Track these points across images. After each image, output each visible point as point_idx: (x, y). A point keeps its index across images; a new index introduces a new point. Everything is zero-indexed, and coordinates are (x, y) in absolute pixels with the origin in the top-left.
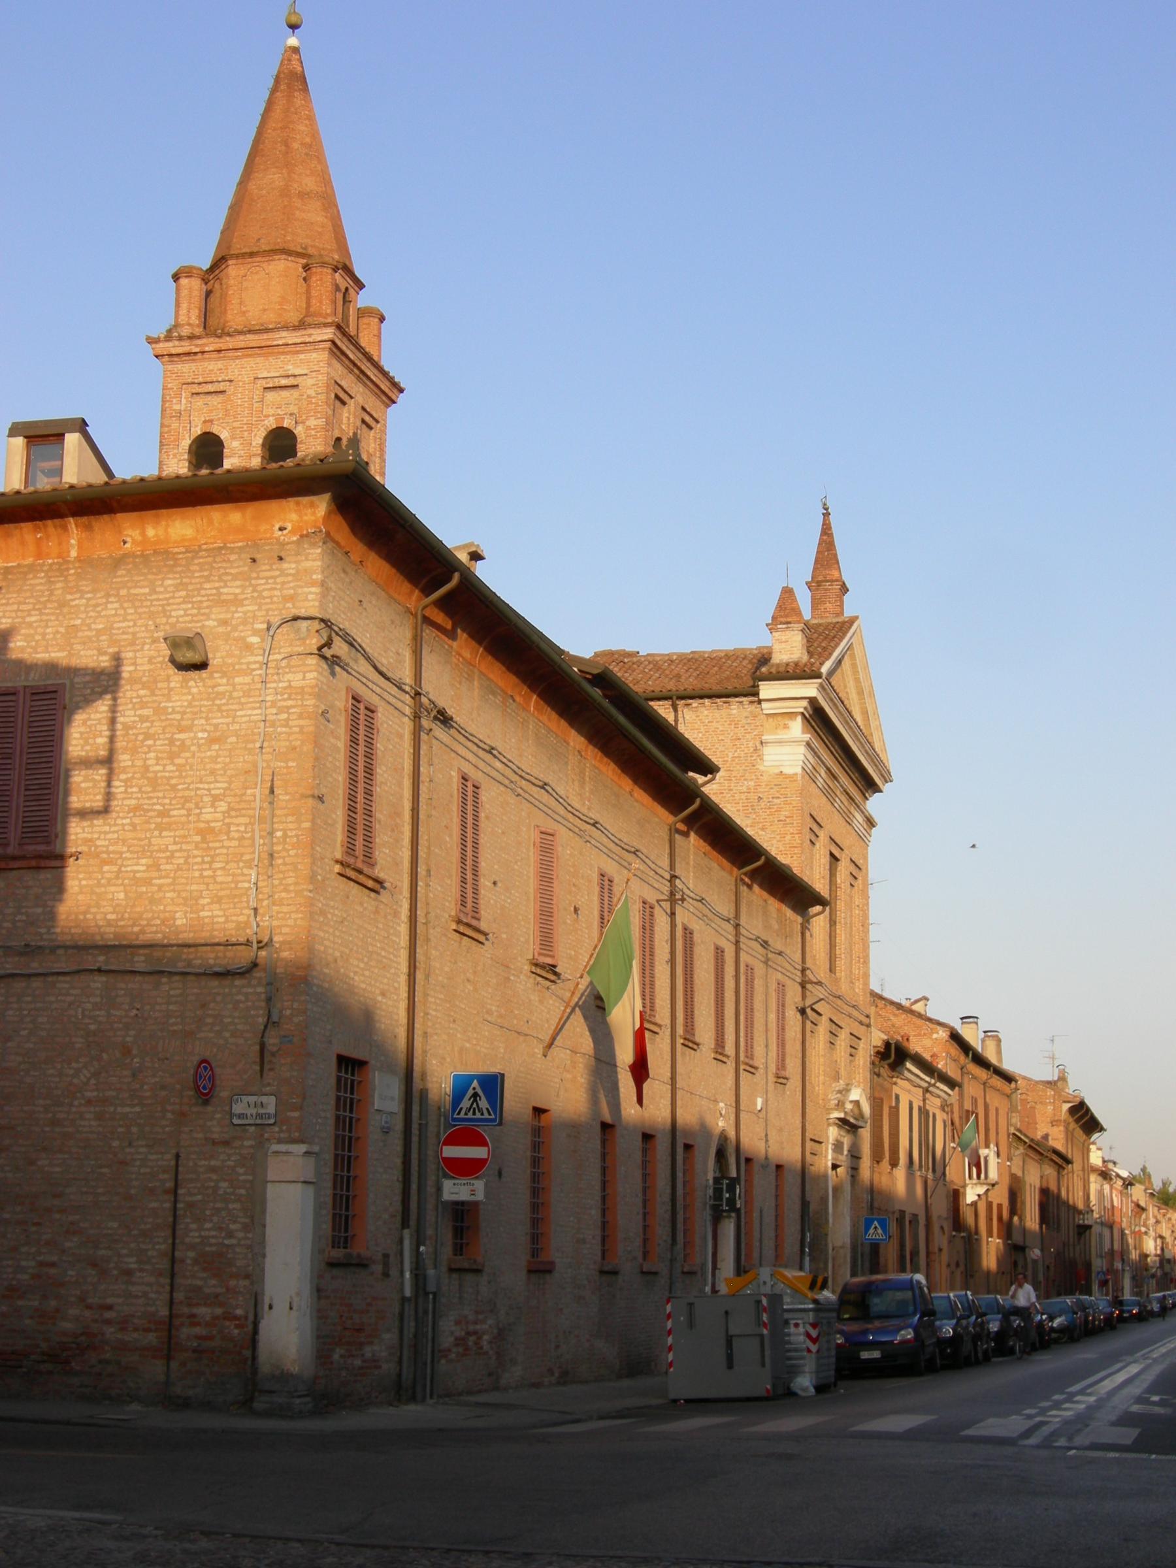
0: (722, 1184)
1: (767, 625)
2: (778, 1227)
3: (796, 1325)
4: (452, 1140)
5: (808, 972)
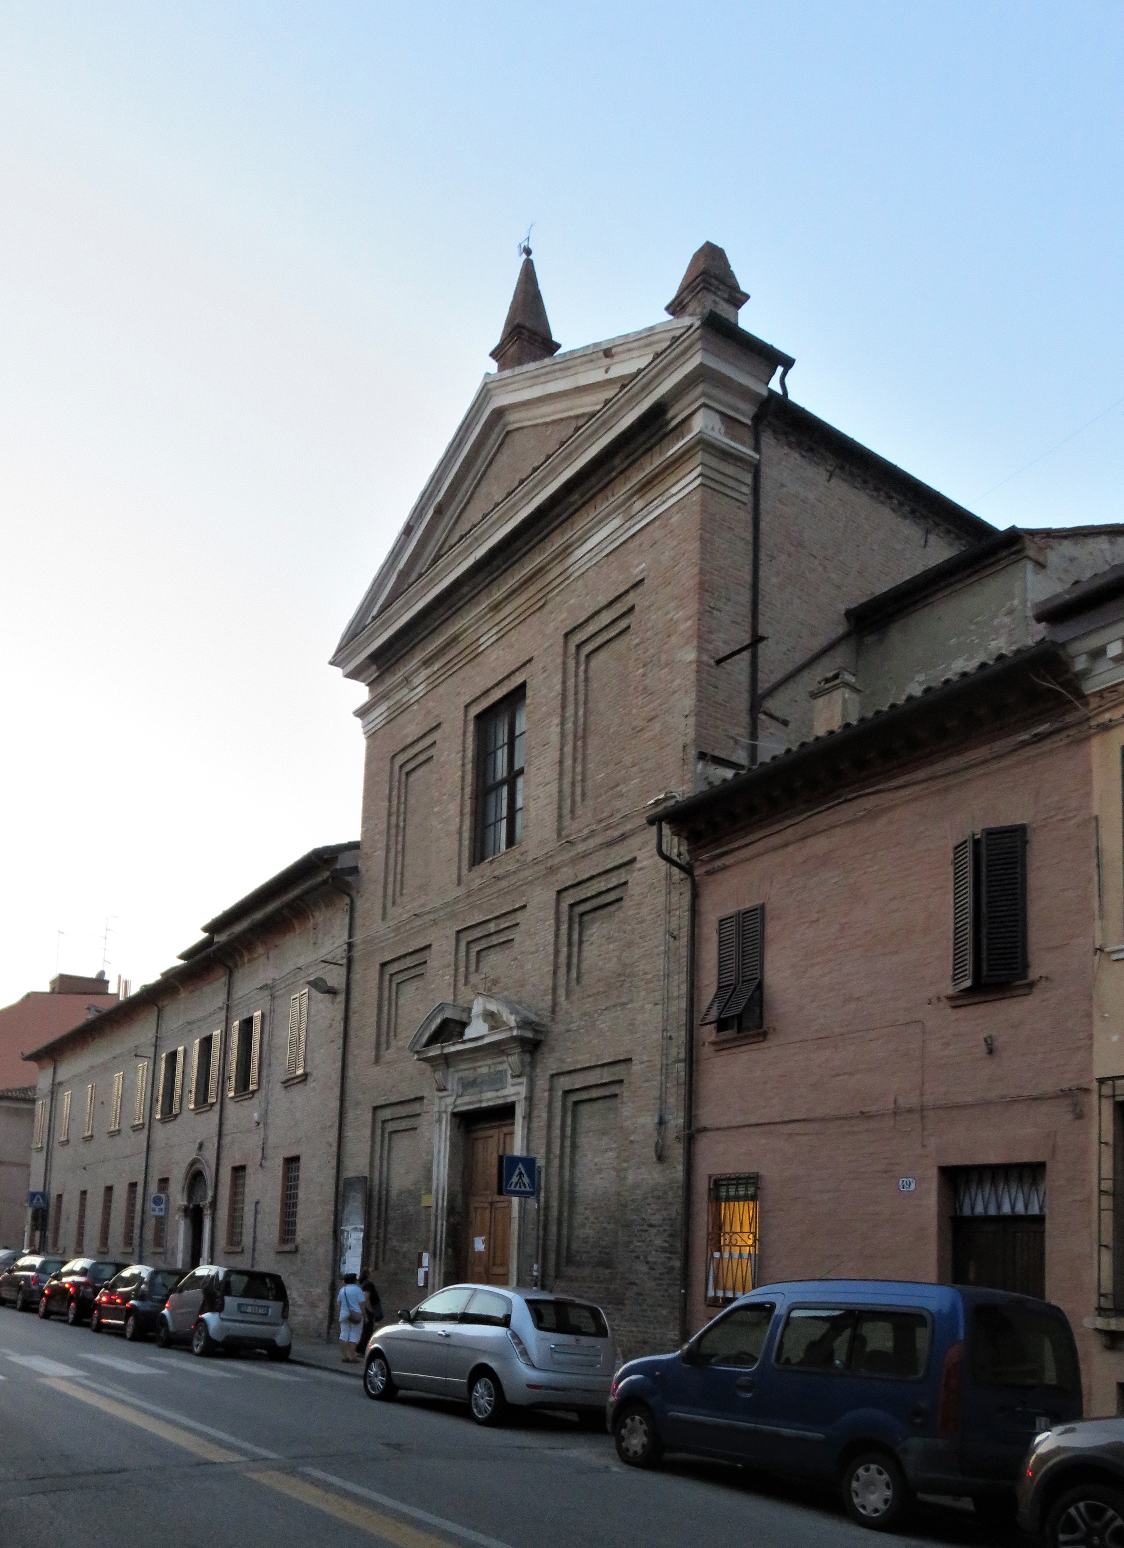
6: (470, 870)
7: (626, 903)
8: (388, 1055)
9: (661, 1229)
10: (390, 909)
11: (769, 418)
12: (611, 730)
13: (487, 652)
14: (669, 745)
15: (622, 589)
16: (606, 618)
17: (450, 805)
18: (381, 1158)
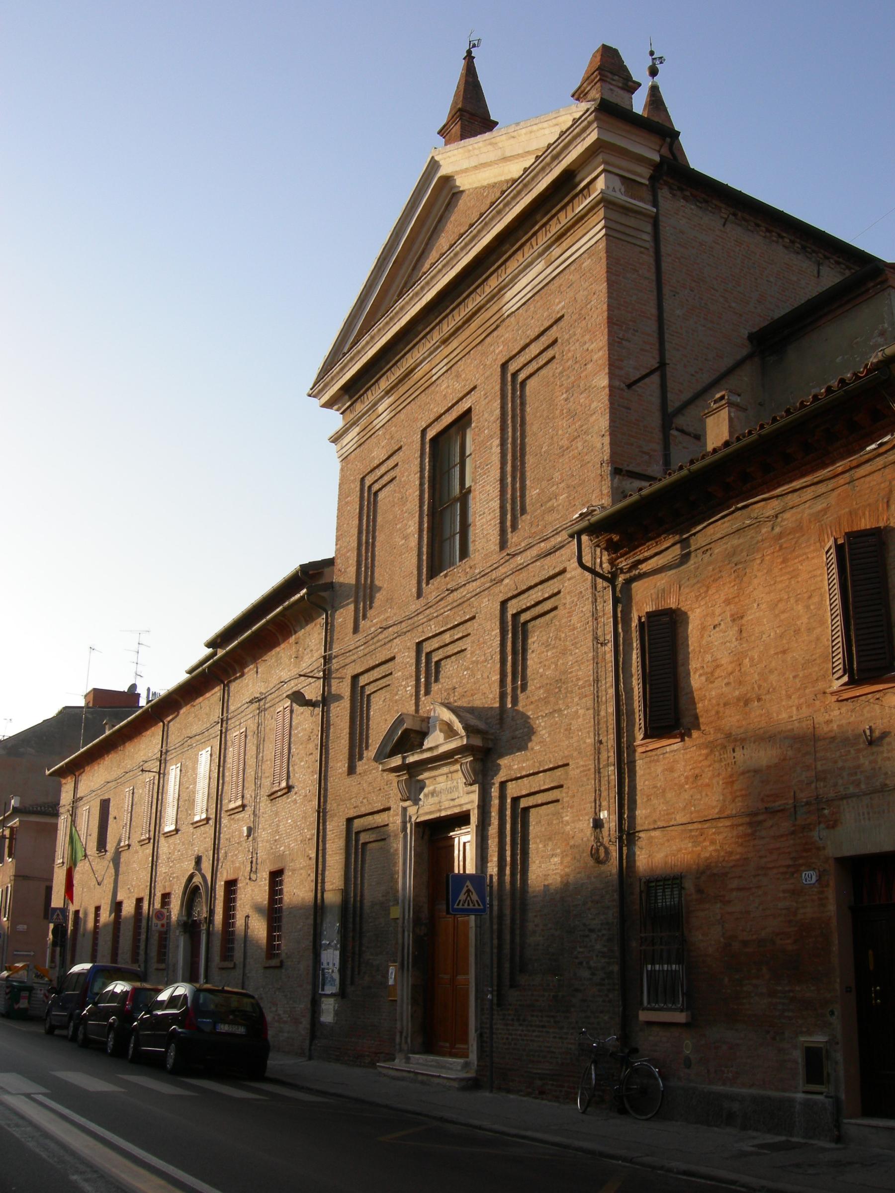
3: (41, 990)
6: (427, 584)
7: (561, 612)
8: (360, 766)
9: (600, 934)
10: (362, 623)
11: (665, 178)
12: (543, 450)
13: (438, 382)
14: (588, 462)
15: (547, 324)
16: (534, 349)
17: (410, 522)
18: (355, 869)
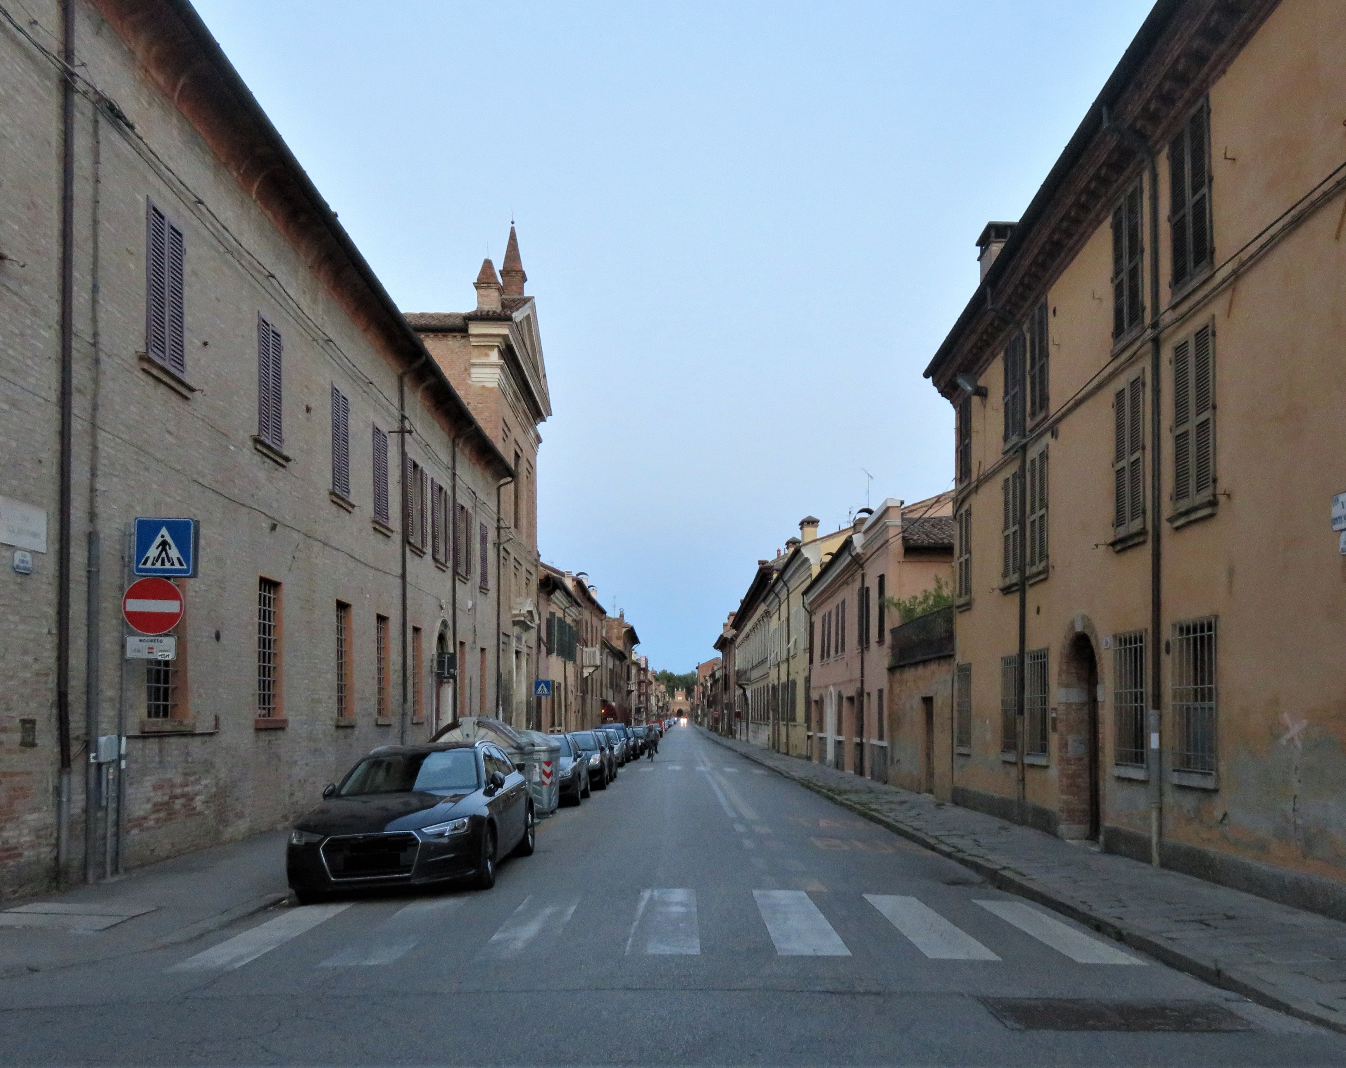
0: (444, 658)
1: (474, 284)
2: (482, 690)
4: (138, 592)
5: (501, 521)
